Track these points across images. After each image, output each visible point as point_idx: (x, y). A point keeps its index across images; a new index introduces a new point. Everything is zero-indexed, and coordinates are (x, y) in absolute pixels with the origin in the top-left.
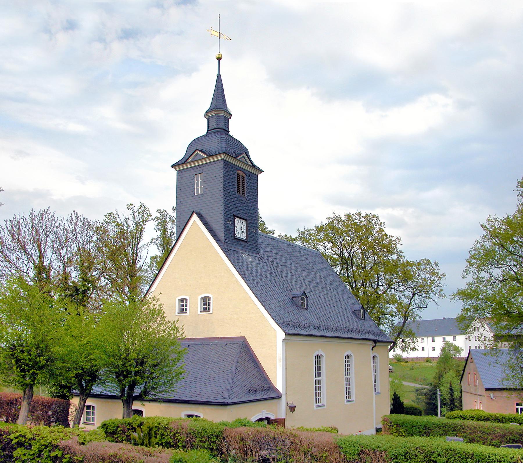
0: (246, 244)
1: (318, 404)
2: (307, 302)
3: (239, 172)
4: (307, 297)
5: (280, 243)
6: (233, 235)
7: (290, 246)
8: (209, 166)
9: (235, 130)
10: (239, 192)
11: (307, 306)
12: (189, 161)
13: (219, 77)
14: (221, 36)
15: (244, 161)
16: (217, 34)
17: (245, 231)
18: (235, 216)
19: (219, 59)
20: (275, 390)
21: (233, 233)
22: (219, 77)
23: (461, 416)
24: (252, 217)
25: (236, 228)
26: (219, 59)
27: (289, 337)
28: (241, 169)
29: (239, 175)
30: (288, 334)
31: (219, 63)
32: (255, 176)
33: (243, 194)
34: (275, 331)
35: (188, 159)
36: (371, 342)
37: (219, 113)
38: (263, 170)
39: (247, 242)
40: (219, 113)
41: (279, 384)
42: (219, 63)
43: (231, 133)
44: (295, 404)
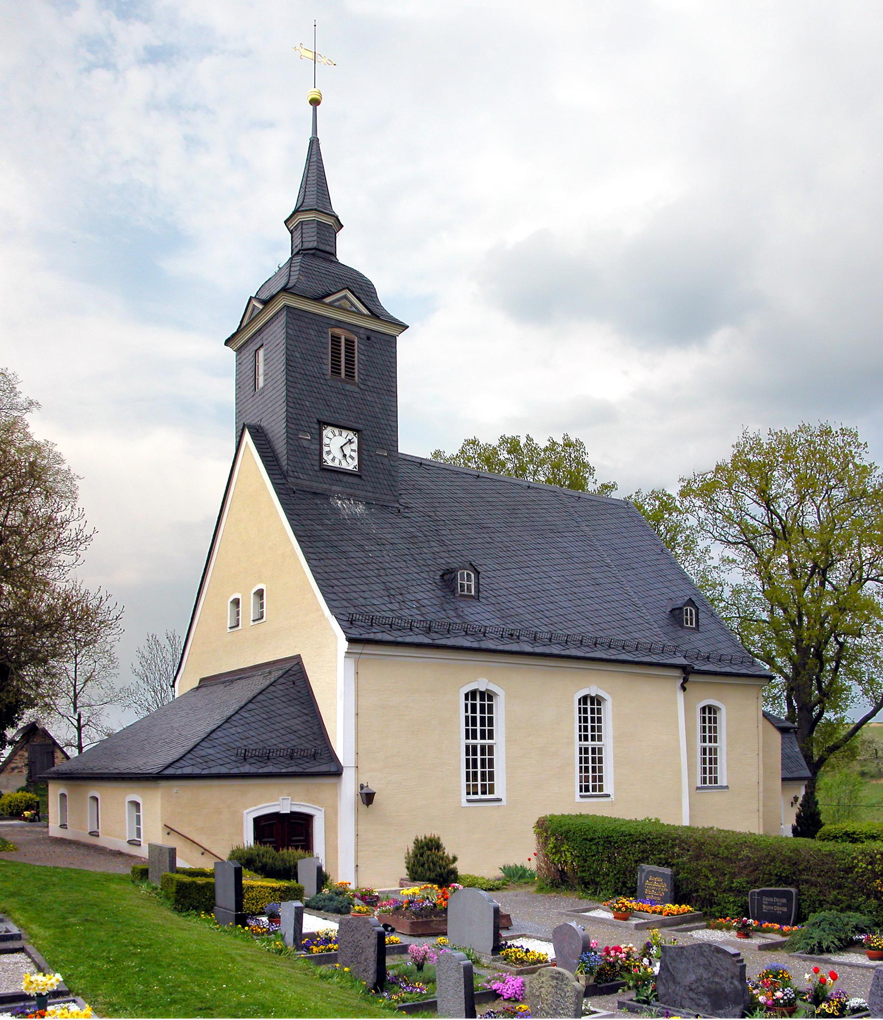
0: (356, 480)
1: (583, 793)
2: (478, 584)
3: (337, 331)
4: (477, 573)
5: (497, 483)
6: (317, 463)
7: (529, 491)
8: (268, 330)
9: (349, 251)
10: (336, 370)
11: (478, 591)
12: (328, 300)
13: (314, 144)
14: (318, 58)
15: (347, 305)
16: (312, 56)
17: (355, 455)
18: (323, 424)
19: (315, 102)
20: (333, 757)
21: (317, 458)
22: (314, 144)
23: (847, 834)
24: (376, 423)
25: (326, 449)
26: (315, 102)
27: (358, 649)
28: (340, 324)
29: (336, 340)
30: (351, 640)
31: (315, 111)
32: (387, 338)
33: (350, 374)
34: (336, 638)
35: (329, 295)
36: (677, 673)
37: (315, 224)
38: (407, 324)
39: (360, 477)
40: (315, 224)
41: (342, 744)
42: (315, 111)
43: (342, 257)
44: (373, 787)
